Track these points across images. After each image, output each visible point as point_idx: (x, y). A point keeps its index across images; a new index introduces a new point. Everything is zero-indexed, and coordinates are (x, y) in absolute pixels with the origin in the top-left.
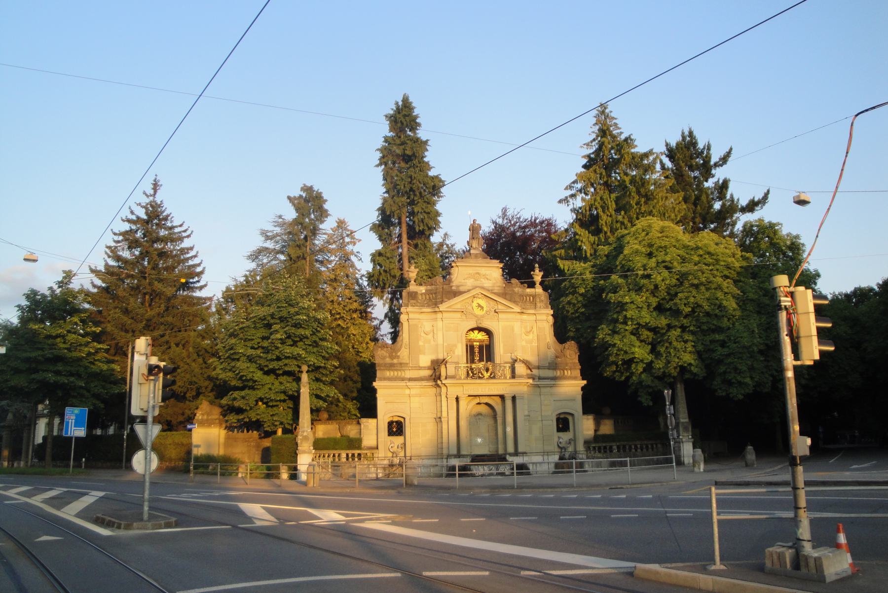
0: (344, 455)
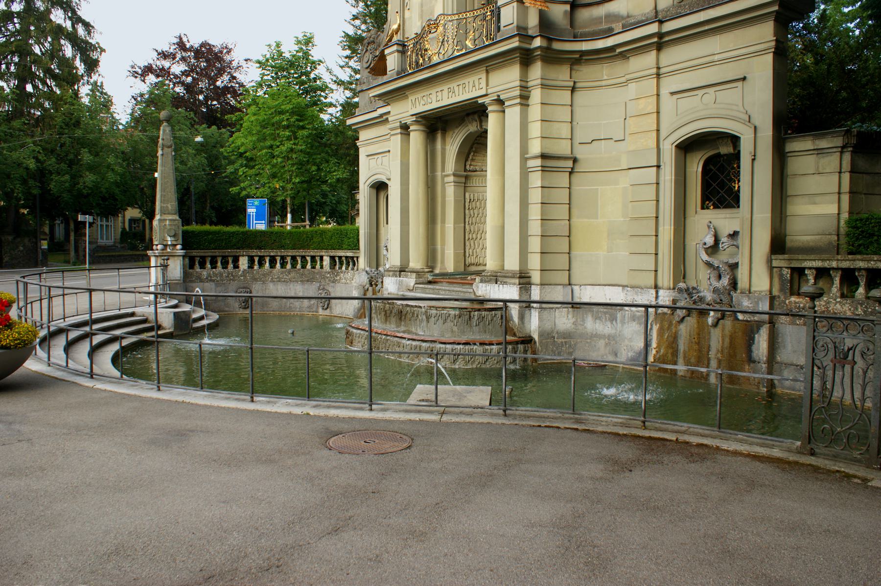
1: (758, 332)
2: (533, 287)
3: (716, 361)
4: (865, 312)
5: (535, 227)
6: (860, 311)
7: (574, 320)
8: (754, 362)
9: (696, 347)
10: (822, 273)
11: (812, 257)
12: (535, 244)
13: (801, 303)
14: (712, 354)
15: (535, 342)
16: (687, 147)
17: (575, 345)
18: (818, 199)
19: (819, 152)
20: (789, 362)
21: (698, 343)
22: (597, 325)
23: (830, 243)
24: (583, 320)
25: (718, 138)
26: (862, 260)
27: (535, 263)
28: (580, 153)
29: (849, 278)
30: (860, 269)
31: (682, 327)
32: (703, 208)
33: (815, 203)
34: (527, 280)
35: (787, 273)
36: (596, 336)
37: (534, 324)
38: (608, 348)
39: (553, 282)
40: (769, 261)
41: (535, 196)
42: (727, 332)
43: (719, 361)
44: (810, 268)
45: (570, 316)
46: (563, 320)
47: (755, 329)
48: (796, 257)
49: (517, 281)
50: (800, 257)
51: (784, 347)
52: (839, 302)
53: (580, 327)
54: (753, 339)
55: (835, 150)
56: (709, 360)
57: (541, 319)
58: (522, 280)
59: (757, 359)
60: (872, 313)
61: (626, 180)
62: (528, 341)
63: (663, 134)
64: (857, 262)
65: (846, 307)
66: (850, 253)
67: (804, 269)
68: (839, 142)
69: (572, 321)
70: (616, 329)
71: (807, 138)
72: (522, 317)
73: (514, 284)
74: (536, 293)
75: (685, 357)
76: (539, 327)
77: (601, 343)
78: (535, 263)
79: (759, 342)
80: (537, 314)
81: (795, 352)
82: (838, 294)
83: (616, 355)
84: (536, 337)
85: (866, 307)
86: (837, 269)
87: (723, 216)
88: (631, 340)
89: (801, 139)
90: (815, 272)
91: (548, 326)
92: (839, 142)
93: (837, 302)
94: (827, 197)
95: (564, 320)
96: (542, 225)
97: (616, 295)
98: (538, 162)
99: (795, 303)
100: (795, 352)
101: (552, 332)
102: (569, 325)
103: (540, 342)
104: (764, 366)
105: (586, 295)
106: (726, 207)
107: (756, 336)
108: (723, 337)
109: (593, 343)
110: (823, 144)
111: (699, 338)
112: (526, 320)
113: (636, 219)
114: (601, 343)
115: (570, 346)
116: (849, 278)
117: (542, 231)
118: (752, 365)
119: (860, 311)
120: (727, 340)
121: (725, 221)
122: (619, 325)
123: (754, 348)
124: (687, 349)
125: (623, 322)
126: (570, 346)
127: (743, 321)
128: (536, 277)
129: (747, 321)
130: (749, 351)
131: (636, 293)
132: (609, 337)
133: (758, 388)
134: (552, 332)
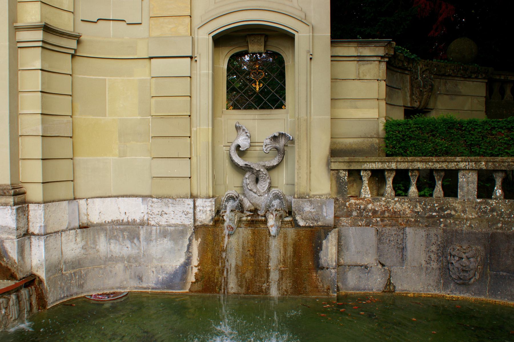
0: (468, 183)
1: (326, 237)
2: (31, 207)
3: (277, 272)
4: (424, 209)
5: (32, 124)
6: (419, 208)
7: (83, 243)
8: (322, 268)
9: (252, 260)
10: (378, 177)
11: (373, 159)
12: (33, 148)
13: (362, 204)
14: (272, 265)
15: (41, 281)
16: (220, 40)
17: (86, 274)
18: (359, 103)
19: (360, 59)
20: (352, 263)
21: (254, 256)
22: (112, 245)
23: (372, 145)
24: (95, 242)
25: (250, 35)
26: (421, 162)
27: (32, 173)
28: (87, 32)
29: (402, 180)
30: (437, 170)
31: (233, 239)
32: (227, 109)
33: (356, 108)
34: (21, 197)
35: (344, 175)
36: (112, 259)
37: (37, 258)
38: (128, 273)
39: (56, 198)
40: (328, 164)
41: (32, 81)
42: (290, 241)
43: (282, 272)
44: (366, 170)
45: (79, 239)
46: (72, 247)
47: (323, 235)
48: (357, 159)
49: (11, 200)
50: (361, 159)
51: (347, 249)
52: (398, 201)
53: (91, 251)
54: (321, 245)
55: (375, 59)
56: (268, 272)
57: (47, 249)
58: (18, 199)
59: (325, 265)
60: (431, 210)
61: (141, 72)
62: (31, 281)
63: (197, 22)
64: (416, 163)
65: (406, 205)
66: (387, 155)
67: (359, 171)
68: (381, 51)
69: (80, 245)
70: (139, 249)
71: (352, 45)
72: (21, 251)
73: (6, 205)
74: (37, 217)
75: (237, 272)
76: (46, 260)
77: (119, 267)
78: (32, 173)
79: (327, 247)
80: (42, 243)
81: (358, 253)
82: (393, 194)
83: (140, 279)
84: (42, 274)
85: (425, 204)
86: (391, 170)
87: (252, 117)
88: (161, 259)
89: (346, 45)
90: (370, 174)
91: (55, 256)
92: (381, 51)
93: (396, 202)
94: (368, 102)
95: (72, 245)
96: (43, 122)
97: (133, 210)
98: (39, 35)
99: (356, 204)
100: (358, 253)
101: (59, 263)
102: (78, 251)
103: (48, 279)
104: (333, 271)
105: (100, 211)
106: (262, 108)
107: (324, 241)
108: (285, 245)
109: (108, 268)
110: (366, 51)
111: (255, 250)
112: (26, 252)
113: (162, 117)
114: (119, 267)
115: (80, 277)
116: (402, 180)
117: (44, 130)
118: (320, 272)
119: (419, 208)
120: (290, 249)
121: (259, 126)
122: (143, 243)
123: (322, 254)
124: (240, 263)
125: (148, 240)
126: (80, 277)
127: (305, 227)
128: (35, 192)
129: (310, 227)
130: (316, 258)
131: (167, 205)
132: (129, 259)
133: (328, 294)
134: (59, 263)
